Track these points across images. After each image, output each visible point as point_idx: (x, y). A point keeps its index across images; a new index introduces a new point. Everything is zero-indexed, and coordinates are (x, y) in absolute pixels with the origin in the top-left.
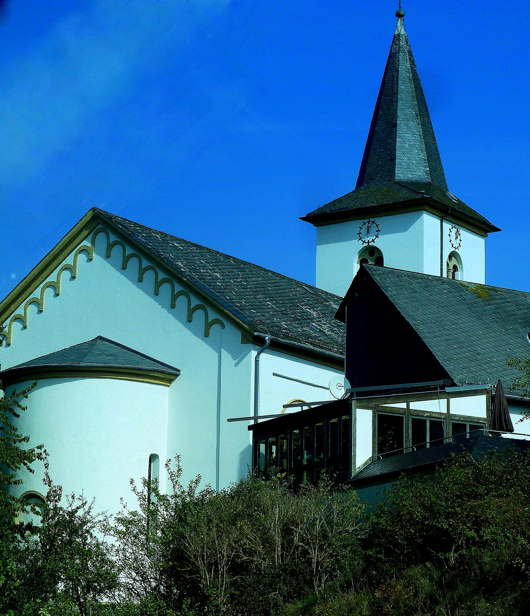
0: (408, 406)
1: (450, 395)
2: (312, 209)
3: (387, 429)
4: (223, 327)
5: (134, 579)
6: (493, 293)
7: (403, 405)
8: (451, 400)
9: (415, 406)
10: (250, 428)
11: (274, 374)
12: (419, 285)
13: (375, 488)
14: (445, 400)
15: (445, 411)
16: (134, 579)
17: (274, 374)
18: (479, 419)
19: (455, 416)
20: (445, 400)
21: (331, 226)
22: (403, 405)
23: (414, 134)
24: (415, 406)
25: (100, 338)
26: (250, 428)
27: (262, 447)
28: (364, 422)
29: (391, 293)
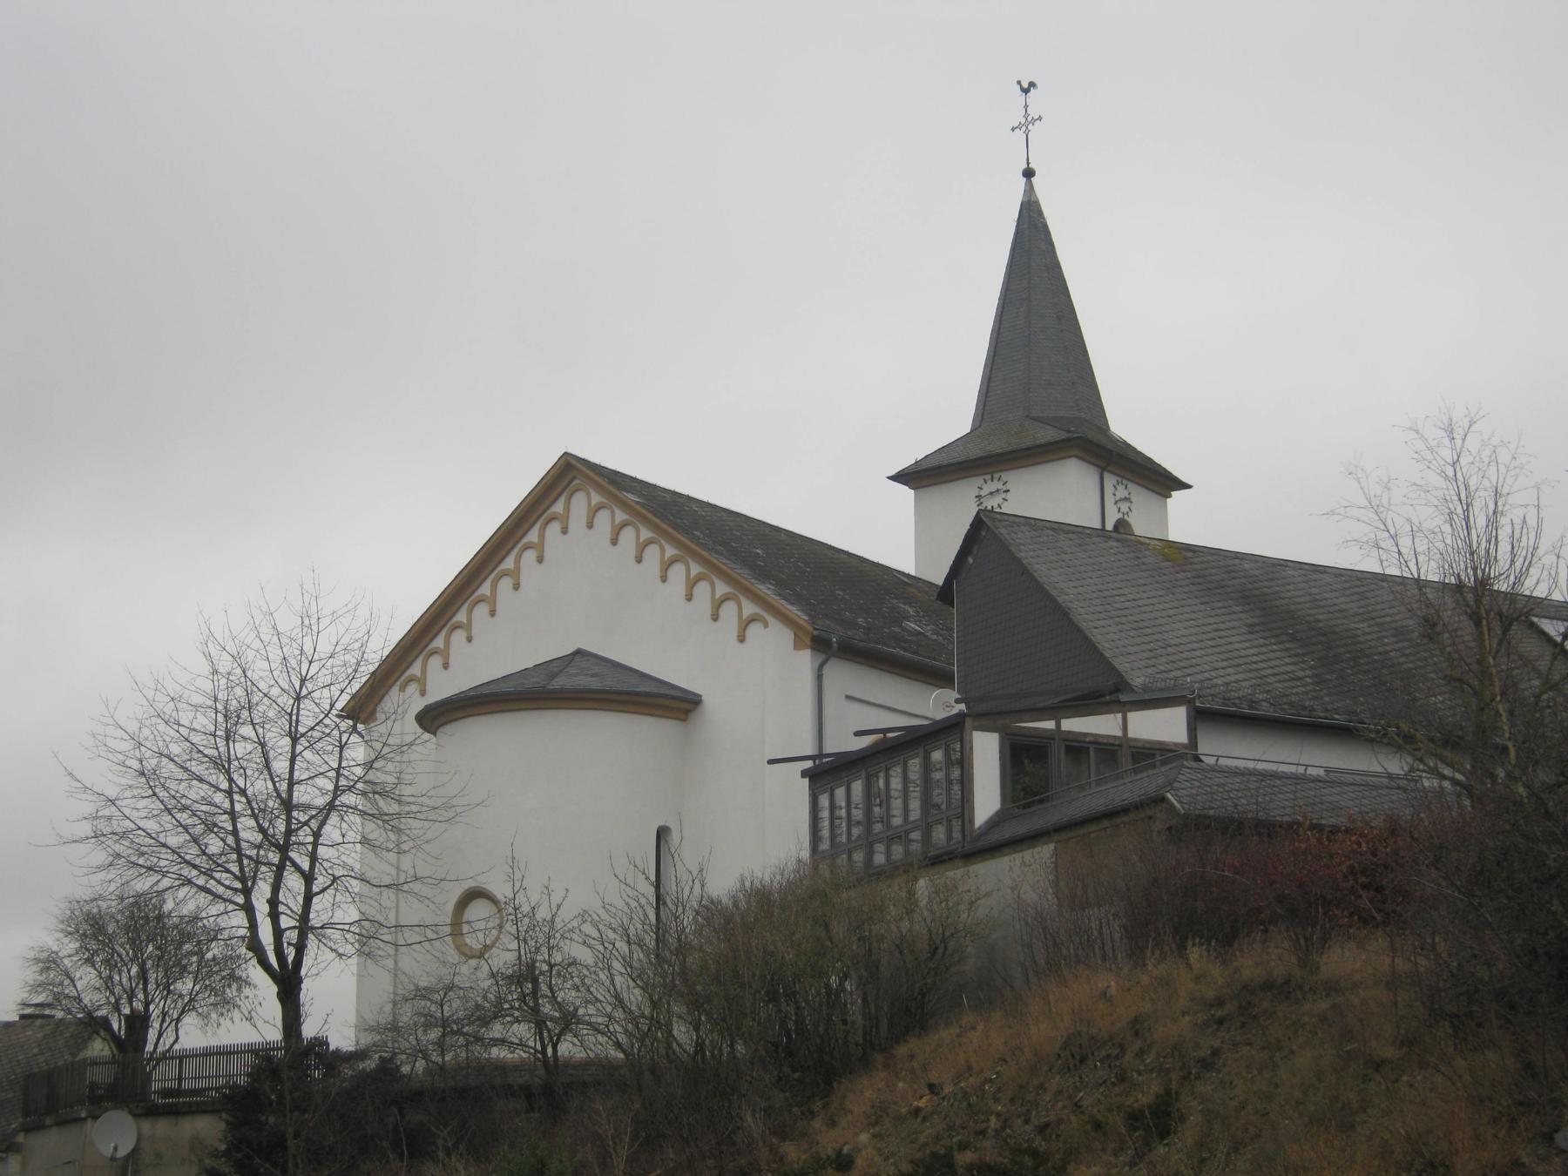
0: (1058, 725)
1: (1125, 707)
2: (905, 461)
3: (1023, 756)
4: (766, 625)
5: (610, 1017)
6: (1190, 554)
7: (1049, 725)
8: (1132, 716)
9: (1072, 725)
10: (804, 774)
11: (771, 762)
12: (1403, 796)
13: (1006, 859)
14: (1119, 716)
15: (1119, 733)
16: (610, 1017)
17: (771, 762)
18: (1176, 744)
19: (1136, 740)
20: (1119, 716)
21: (943, 487)
22: (1049, 725)
23: (938, 1138)
24: (1072, 725)
25: (579, 652)
26: (804, 774)
27: (824, 801)
28: (986, 750)
29: (1026, 554)
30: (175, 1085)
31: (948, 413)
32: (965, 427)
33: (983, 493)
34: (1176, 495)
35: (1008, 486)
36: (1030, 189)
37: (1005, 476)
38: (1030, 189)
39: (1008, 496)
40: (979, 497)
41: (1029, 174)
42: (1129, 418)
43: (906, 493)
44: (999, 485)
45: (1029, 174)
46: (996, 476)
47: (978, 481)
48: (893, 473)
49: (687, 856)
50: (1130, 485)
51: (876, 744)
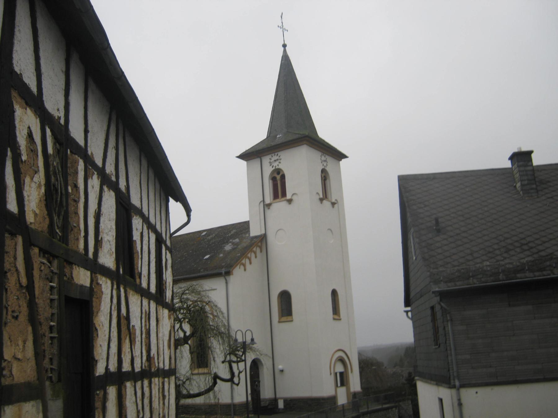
8: (463, 391)
30: (104, 359)
31: (258, 132)
32: (265, 137)
33: (271, 161)
34: (344, 161)
35: (281, 157)
36: (285, 51)
37: (280, 153)
38: (285, 51)
39: (281, 161)
40: (270, 162)
41: (284, 46)
42: (325, 131)
43: (243, 163)
44: (278, 157)
45: (284, 46)
46: (276, 154)
47: (269, 156)
48: (238, 155)
49: (213, 292)
50: (326, 156)
51: (159, 232)
